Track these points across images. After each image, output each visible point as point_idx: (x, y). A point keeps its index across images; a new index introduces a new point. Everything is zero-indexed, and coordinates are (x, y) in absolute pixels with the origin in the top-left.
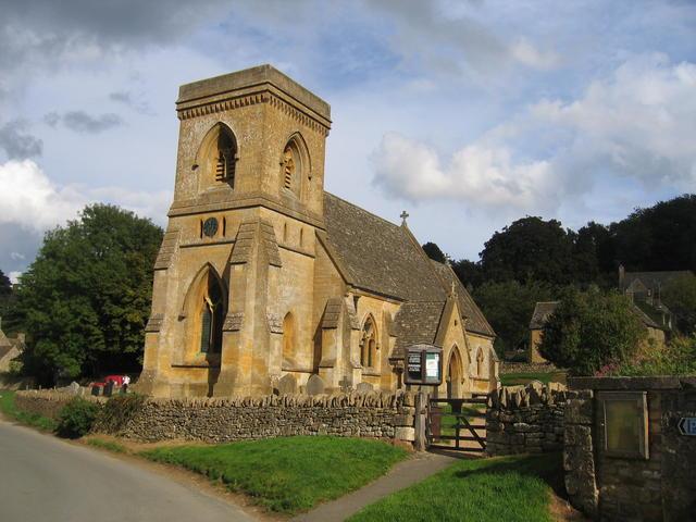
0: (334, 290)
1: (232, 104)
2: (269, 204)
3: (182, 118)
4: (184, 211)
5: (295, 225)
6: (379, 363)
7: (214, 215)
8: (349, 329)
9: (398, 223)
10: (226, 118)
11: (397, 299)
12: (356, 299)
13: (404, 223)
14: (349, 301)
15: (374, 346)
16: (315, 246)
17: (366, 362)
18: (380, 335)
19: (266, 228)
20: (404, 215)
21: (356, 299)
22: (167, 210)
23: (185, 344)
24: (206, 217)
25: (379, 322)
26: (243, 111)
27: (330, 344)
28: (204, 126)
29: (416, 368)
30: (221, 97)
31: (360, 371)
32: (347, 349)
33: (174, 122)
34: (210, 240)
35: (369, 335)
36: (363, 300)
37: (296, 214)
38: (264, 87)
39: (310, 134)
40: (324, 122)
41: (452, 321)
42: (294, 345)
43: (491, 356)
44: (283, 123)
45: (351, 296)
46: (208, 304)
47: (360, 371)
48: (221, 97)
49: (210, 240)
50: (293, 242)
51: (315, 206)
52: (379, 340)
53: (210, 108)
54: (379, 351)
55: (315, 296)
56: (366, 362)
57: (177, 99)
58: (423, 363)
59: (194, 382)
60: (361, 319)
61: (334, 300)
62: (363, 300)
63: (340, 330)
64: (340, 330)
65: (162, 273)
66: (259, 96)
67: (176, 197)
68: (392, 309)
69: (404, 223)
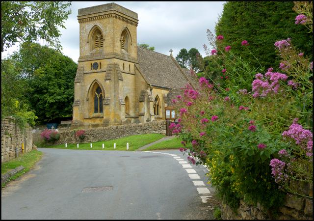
0: (143, 87)
1: (100, 18)
2: (117, 57)
3: (80, 22)
4: (83, 60)
5: (127, 64)
6: (161, 114)
7: (96, 61)
8: (149, 101)
12: (151, 90)
13: (171, 54)
14: (149, 91)
15: (159, 107)
21: (151, 90)
24: (93, 62)
25: (161, 98)
26: (105, 21)
28: (89, 26)
32: (149, 109)
34: (96, 71)
35: (157, 103)
36: (154, 90)
37: (127, 59)
39: (130, 27)
40: (136, 21)
42: (129, 108)
44: (121, 25)
48: (95, 15)
49: (94, 71)
50: (127, 70)
52: (161, 104)
53: (91, 19)
55: (136, 89)
59: (93, 123)
60: (153, 97)
62: (154, 90)
63: (146, 102)
64: (146, 102)
68: (166, 92)
69: (171, 54)
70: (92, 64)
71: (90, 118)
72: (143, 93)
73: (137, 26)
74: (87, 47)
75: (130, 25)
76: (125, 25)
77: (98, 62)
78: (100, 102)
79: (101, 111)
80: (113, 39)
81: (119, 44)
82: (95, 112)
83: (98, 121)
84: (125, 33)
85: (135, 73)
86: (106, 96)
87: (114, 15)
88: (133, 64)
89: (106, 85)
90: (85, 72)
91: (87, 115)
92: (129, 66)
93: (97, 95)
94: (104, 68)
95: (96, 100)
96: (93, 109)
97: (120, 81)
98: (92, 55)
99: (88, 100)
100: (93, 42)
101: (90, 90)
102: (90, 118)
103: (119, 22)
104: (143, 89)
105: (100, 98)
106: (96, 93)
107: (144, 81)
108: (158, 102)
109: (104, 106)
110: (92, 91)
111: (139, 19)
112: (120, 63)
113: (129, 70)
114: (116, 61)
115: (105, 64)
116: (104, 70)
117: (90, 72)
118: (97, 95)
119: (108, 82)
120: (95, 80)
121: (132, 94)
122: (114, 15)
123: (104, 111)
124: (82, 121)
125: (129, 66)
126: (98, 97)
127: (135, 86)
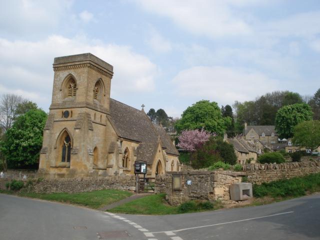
0: (113, 138)
1: (75, 67)
2: (89, 106)
7: (68, 110)
9: (140, 109)
10: (72, 72)
11: (137, 142)
12: (121, 142)
14: (119, 143)
15: (128, 160)
16: (106, 121)
17: (125, 165)
18: (131, 155)
19: (88, 115)
20: (143, 106)
21: (121, 142)
22: (49, 107)
23: (57, 158)
24: (64, 110)
25: (130, 150)
26: (80, 70)
28: (64, 75)
29: (138, 168)
30: (71, 64)
31: (122, 170)
33: (53, 72)
34: (66, 119)
35: (126, 156)
36: (124, 142)
37: (99, 110)
38: (88, 62)
39: (104, 78)
40: (111, 73)
41: (158, 151)
43: (178, 163)
44: (96, 76)
45: (120, 141)
46: (65, 144)
47: (122, 170)
48: (71, 64)
50: (98, 120)
51: (106, 106)
53: (66, 68)
54: (130, 162)
56: (125, 165)
58: (140, 167)
59: (59, 173)
61: (113, 142)
65: (47, 131)
66: (86, 65)
67: (52, 102)
68: (135, 145)
69: (143, 109)
71: (56, 167)
72: (113, 146)
73: (112, 78)
74: (60, 95)
75: (105, 77)
76: (99, 76)
77: (69, 110)
79: (69, 160)
80: (87, 91)
81: (92, 94)
82: (243, 191)
83: (64, 171)
84: (98, 83)
85: (106, 123)
86: (74, 145)
87: (88, 65)
88: (106, 115)
89: (75, 134)
90: (55, 120)
91: (53, 163)
92: (101, 116)
93: (66, 143)
94: (75, 117)
95: (64, 149)
96: (61, 158)
97: (90, 131)
98: (64, 103)
100: (66, 91)
102: (56, 167)
103: (94, 72)
106: (65, 142)
107: (115, 133)
108: (127, 154)
109: (71, 155)
110: (61, 139)
111: (114, 71)
112: (92, 112)
113: (101, 121)
114: (88, 110)
115: (77, 112)
116: (75, 119)
118: (66, 143)
120: (65, 128)
121: (102, 145)
122: (88, 65)
123: (71, 161)
124: (48, 169)
125: (101, 116)
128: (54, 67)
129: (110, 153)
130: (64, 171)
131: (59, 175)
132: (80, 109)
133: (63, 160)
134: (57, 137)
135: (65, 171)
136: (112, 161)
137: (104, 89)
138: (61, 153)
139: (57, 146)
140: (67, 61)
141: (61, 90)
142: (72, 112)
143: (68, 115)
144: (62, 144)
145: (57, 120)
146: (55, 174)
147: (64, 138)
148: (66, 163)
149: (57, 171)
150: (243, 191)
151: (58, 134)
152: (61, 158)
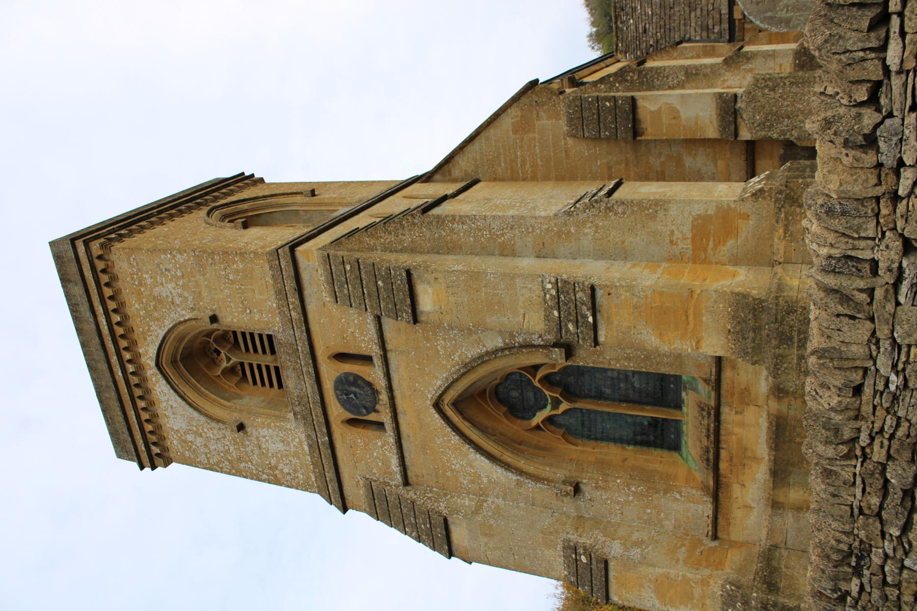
22: (334, 511)
24: (337, 411)
25: (831, 281)
26: (134, 307)
27: (675, 115)
34: (384, 397)
46: (550, 420)
57: (135, 465)
59: (760, 473)
63: (636, 94)
64: (636, 94)
70: (351, 422)
71: (717, 492)
77: (330, 372)
78: (599, 396)
79: (664, 389)
82: (675, 446)
83: (750, 429)
95: (582, 430)
96: (655, 460)
99: (577, 489)
101: (508, 457)
102: (717, 492)
104: (563, 125)
105: (569, 393)
110: (514, 444)
115: (341, 325)
117: (389, 437)
119: (427, 301)
120: (437, 406)
126: (564, 406)
127: (546, 178)
128: (154, 467)
129: (636, 131)
130: (750, 429)
131: (780, 474)
132: (307, 292)
133: (661, 437)
134: (498, 473)
135: (750, 414)
136: (688, 113)
137: (282, 200)
138: (613, 452)
139: (560, 475)
140: (113, 394)
141: (241, 427)
142: (341, 357)
143: (356, 380)
144: (549, 437)
145: (394, 461)
146: (775, 505)
147: (513, 427)
148: (690, 419)
149: (750, 489)
150: (675, 446)
151: (482, 462)
152: (657, 453)
